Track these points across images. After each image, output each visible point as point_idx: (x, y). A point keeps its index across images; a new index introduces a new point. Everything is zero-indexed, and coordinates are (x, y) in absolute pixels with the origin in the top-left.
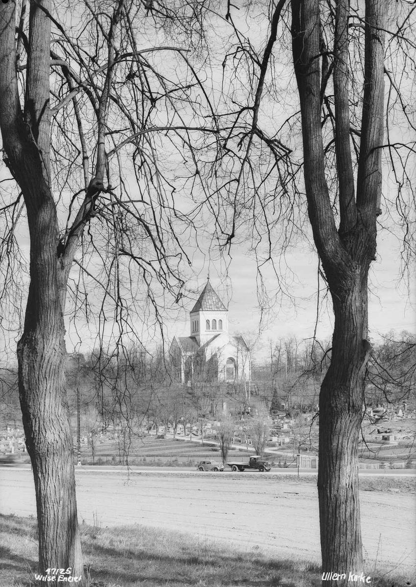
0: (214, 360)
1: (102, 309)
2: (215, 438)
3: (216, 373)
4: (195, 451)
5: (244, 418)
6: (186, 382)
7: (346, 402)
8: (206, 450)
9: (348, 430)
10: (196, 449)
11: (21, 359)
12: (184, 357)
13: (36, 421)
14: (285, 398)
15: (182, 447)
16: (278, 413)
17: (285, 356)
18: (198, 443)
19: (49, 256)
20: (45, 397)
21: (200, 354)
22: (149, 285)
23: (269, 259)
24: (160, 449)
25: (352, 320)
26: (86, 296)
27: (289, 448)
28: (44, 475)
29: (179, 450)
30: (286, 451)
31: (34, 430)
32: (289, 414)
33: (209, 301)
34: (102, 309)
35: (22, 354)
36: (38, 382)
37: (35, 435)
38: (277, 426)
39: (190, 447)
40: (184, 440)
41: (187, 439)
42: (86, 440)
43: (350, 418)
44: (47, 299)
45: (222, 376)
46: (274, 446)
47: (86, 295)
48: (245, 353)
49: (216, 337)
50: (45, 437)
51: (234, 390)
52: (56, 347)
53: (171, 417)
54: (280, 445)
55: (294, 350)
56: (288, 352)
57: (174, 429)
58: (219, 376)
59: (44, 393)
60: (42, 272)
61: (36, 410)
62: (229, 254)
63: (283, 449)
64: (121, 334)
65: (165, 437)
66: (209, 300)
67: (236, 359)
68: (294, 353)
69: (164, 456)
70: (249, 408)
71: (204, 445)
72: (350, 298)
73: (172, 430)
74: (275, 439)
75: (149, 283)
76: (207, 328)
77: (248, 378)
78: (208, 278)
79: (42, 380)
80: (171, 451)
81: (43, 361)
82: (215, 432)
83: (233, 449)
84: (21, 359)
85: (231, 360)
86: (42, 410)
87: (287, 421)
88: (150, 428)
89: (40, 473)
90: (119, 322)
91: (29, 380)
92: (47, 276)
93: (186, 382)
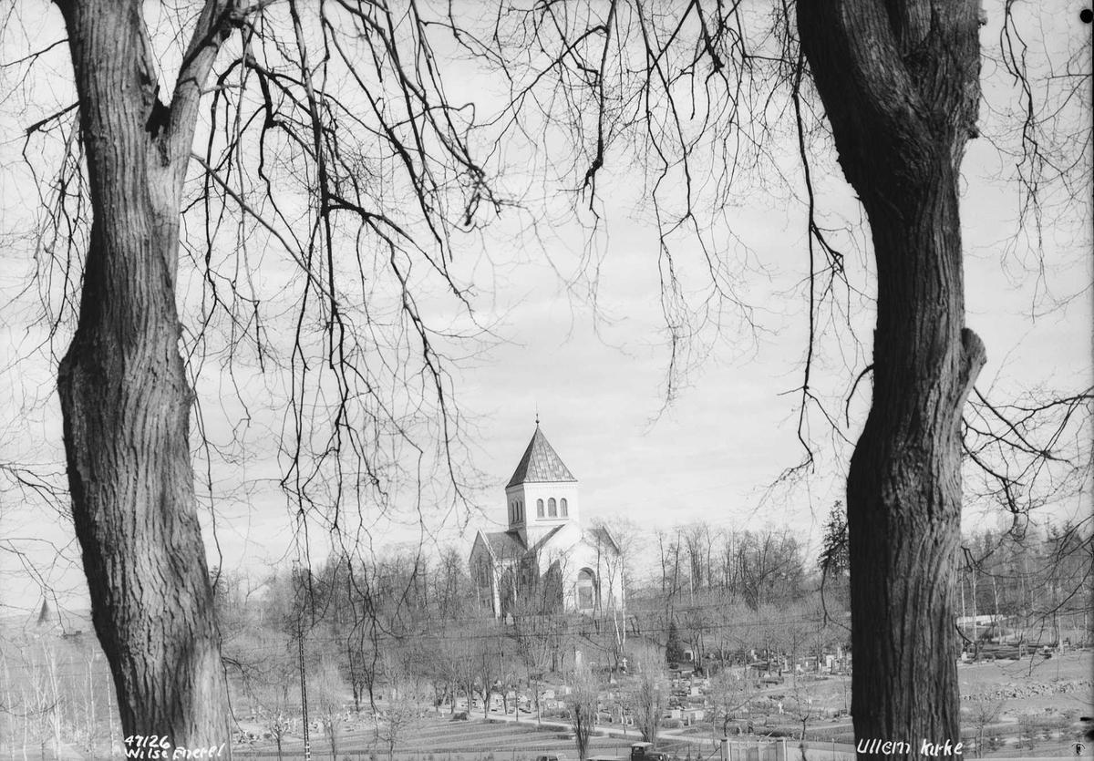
0: (554, 574)
1: (297, 343)
2: (564, 716)
3: (560, 596)
4: (526, 740)
5: (615, 678)
6: (504, 616)
7: (923, 492)
8: (546, 738)
9: (930, 566)
10: (529, 736)
11: (68, 401)
12: (499, 571)
13: (114, 564)
14: (692, 642)
15: (500, 734)
16: (679, 669)
17: (688, 562)
18: (532, 725)
19: (122, 116)
20: (134, 498)
21: (528, 561)
22: (403, 283)
23: (687, 216)
24: (458, 739)
25: (934, 272)
26: (256, 306)
27: (705, 729)
28: (144, 701)
29: (498, 739)
30: (700, 734)
31: (111, 586)
32: (701, 670)
33: (542, 464)
34: (297, 343)
35: (70, 387)
36: (113, 461)
37: (116, 598)
38: (679, 692)
39: (516, 732)
40: (504, 722)
41: (509, 719)
42: (321, 726)
43: (934, 535)
44: (123, 235)
45: (570, 602)
46: (675, 726)
47: (256, 304)
48: (611, 558)
49: (556, 530)
50: (139, 604)
51: (594, 628)
52: (155, 365)
53: (478, 681)
54: (686, 725)
55: (705, 550)
56: (694, 555)
57: (485, 702)
58: (565, 603)
59: (131, 487)
60: (106, 158)
61: (114, 532)
62: (591, 208)
63: (692, 731)
64: (344, 401)
65: (468, 717)
66: (539, 464)
67: (595, 570)
68: (705, 556)
69: (468, 750)
70: (625, 660)
71: (541, 728)
72: (929, 210)
73: (481, 705)
74: (676, 714)
75: (404, 280)
76: (538, 515)
77: (619, 605)
78: (537, 422)
79: (125, 454)
80: (481, 741)
81: (123, 403)
82: (561, 705)
83: (599, 734)
84: (68, 401)
85: (587, 572)
86: (129, 533)
87: (696, 681)
88: (440, 702)
89: (132, 697)
90: (338, 368)
91: (89, 454)
92: (119, 170)
93: (504, 616)
